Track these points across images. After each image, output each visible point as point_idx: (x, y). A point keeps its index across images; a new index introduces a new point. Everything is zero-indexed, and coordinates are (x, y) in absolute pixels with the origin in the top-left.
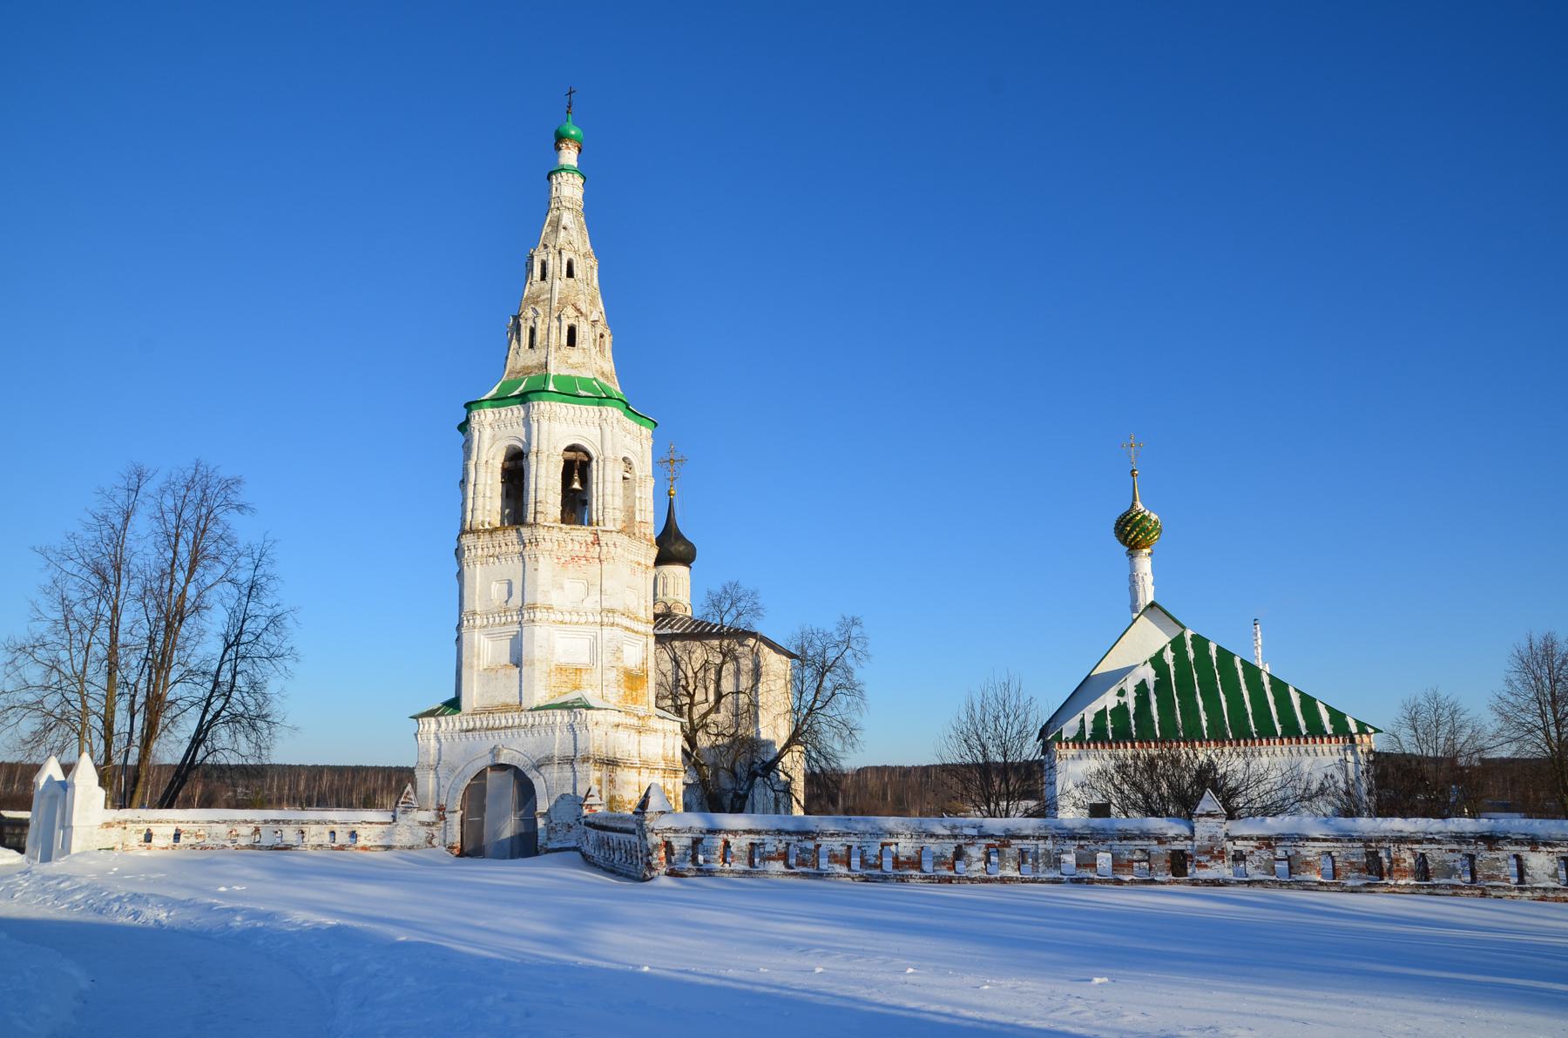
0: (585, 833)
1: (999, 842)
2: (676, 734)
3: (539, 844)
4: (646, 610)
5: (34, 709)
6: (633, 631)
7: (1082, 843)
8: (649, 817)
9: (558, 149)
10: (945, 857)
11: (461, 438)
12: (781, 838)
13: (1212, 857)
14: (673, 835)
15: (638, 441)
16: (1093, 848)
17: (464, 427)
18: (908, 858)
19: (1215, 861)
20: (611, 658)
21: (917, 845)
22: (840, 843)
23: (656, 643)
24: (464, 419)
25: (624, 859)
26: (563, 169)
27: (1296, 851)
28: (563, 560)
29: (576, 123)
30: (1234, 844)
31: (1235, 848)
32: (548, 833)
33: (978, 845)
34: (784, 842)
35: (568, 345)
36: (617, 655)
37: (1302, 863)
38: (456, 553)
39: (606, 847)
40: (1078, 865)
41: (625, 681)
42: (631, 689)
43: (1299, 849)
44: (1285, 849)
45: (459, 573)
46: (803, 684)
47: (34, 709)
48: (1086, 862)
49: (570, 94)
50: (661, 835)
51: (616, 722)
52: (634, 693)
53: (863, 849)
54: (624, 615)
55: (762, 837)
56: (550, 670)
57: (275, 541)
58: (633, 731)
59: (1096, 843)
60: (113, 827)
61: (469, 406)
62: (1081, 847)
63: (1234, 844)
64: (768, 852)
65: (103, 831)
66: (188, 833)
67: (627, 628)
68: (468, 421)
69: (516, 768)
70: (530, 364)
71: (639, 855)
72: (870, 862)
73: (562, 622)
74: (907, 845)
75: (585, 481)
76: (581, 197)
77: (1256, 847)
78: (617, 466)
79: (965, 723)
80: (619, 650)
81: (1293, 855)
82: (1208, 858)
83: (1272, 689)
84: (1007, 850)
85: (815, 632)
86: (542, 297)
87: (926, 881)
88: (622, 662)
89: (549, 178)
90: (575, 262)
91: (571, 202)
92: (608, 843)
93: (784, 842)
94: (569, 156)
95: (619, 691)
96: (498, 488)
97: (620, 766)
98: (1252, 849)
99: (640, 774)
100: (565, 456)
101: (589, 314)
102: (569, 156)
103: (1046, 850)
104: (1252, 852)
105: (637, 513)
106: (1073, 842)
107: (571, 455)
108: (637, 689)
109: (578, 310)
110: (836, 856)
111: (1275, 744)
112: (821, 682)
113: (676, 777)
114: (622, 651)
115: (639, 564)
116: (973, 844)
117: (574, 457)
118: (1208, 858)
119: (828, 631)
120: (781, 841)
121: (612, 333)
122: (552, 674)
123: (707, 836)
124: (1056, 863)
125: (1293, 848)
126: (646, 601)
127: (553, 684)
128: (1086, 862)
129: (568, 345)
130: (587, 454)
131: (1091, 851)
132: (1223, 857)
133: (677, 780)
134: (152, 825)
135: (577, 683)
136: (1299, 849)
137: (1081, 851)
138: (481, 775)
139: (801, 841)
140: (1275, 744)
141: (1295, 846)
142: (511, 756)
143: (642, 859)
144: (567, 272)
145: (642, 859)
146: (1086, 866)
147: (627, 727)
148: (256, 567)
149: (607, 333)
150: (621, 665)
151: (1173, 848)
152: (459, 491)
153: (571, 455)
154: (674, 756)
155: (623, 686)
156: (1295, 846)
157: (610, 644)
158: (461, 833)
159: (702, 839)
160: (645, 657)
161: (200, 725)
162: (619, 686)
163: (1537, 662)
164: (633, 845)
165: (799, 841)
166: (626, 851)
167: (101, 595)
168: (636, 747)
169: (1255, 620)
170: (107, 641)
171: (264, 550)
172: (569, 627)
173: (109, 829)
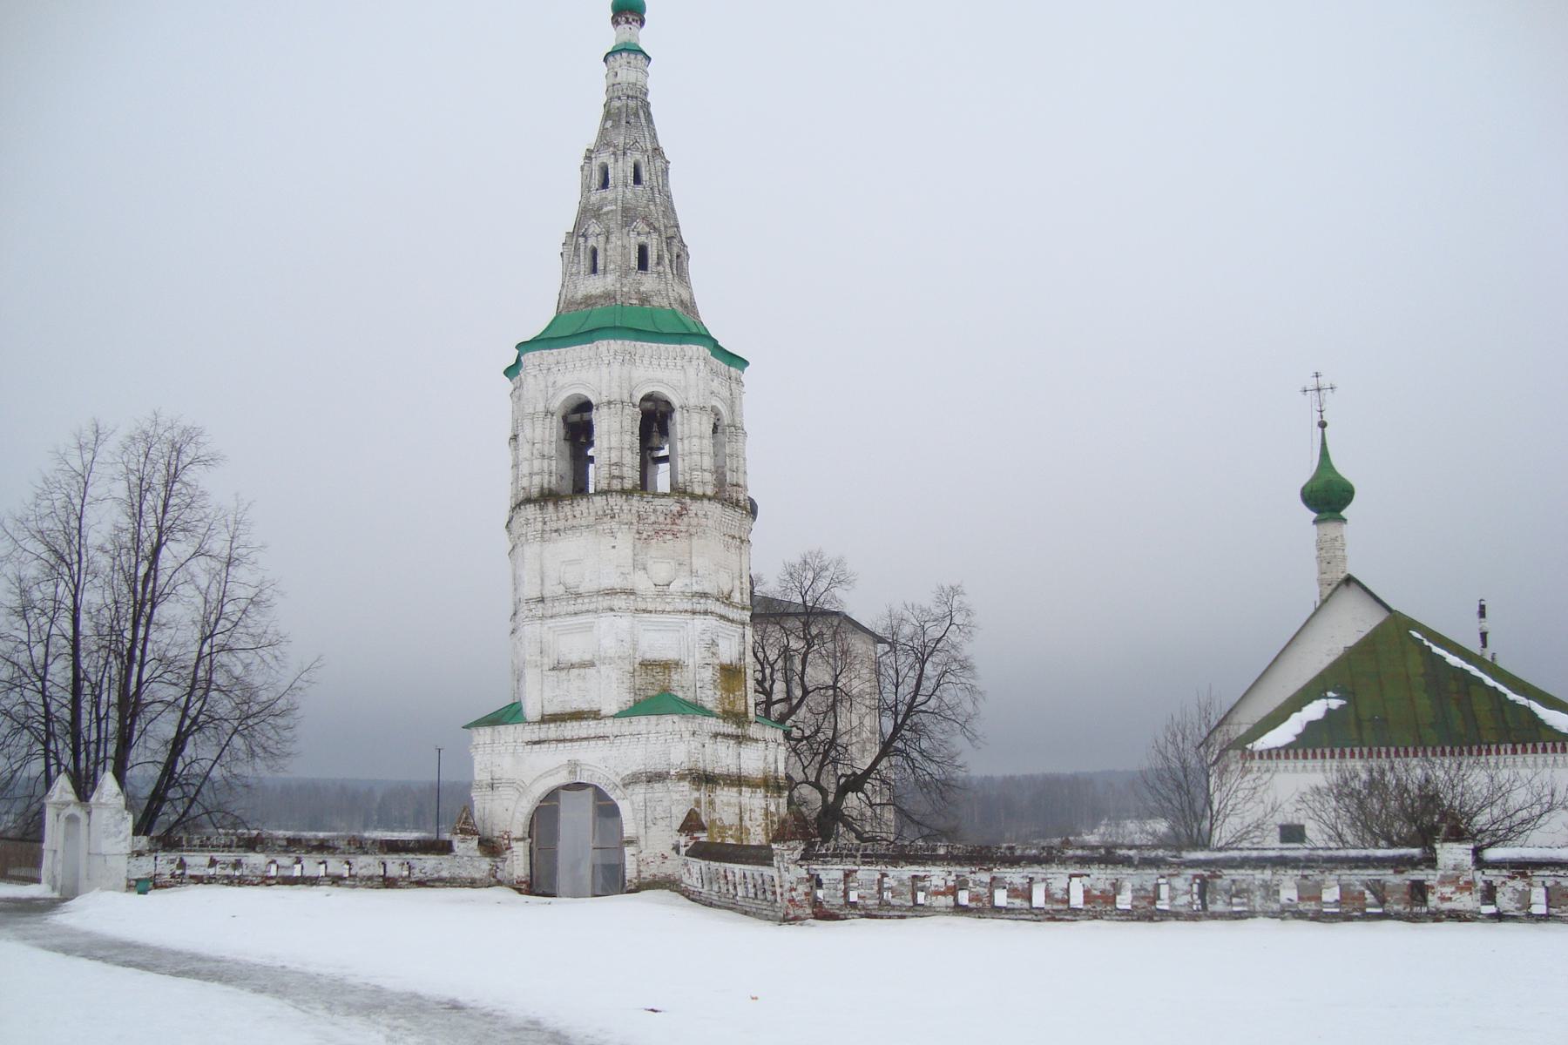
0: (686, 865)
1: (1208, 873)
2: (779, 744)
3: (627, 878)
4: (742, 594)
5: (1222, 824)
6: (728, 620)
7: (1307, 872)
10: (1145, 890)
11: (508, 386)
12: (950, 869)
13: (1457, 888)
14: (821, 867)
15: (727, 386)
16: (1319, 878)
18: (1103, 892)
19: (1461, 893)
20: (706, 654)
21: (1113, 877)
22: (1022, 875)
27: (1556, 881)
28: (644, 535)
30: (1483, 873)
31: (1484, 878)
32: (638, 865)
33: (1184, 876)
34: (953, 874)
36: (713, 650)
37: (1563, 895)
39: (722, 881)
40: (1300, 898)
41: (722, 681)
42: (728, 690)
43: (1559, 880)
44: (1543, 879)
46: (898, 675)
47: (1222, 824)
48: (1310, 893)
50: (806, 867)
52: (731, 696)
53: (1049, 881)
54: (719, 600)
55: (927, 868)
56: (634, 670)
57: (655, 585)
58: (733, 742)
59: (1322, 872)
60: (143, 855)
62: (1305, 877)
63: (1483, 873)
64: (936, 886)
65: (133, 860)
66: (224, 864)
67: (722, 617)
69: (596, 787)
70: (593, 293)
71: (778, 890)
72: (1056, 896)
73: (644, 611)
74: (1100, 876)
77: (1509, 877)
78: (705, 418)
79: (131, 574)
80: (714, 643)
81: (1552, 887)
82: (1453, 889)
83: (1467, 672)
84: (1218, 881)
85: (910, 607)
86: (605, 209)
87: (1122, 918)
88: (718, 658)
92: (726, 877)
93: (953, 874)
95: (715, 694)
97: (719, 784)
98: (1504, 879)
99: (740, 794)
100: (643, 407)
101: (662, 229)
103: (1263, 880)
104: (1504, 883)
105: (728, 474)
106: (1296, 872)
108: (734, 691)
110: (1015, 890)
111: (1506, 753)
112: (922, 670)
113: (780, 797)
114: (718, 646)
115: (734, 537)
116: (1177, 875)
117: (653, 408)
118: (1453, 889)
119: (925, 606)
120: (950, 873)
122: (636, 674)
123: (862, 867)
124: (1271, 891)
125: (1552, 878)
126: (741, 583)
127: (637, 687)
128: (1310, 893)
131: (1316, 881)
132: (1470, 889)
133: (781, 800)
134: (184, 854)
135: (666, 684)
136: (1559, 880)
137: (1305, 881)
138: (552, 795)
139: (974, 873)
140: (1506, 753)
141: (1555, 876)
142: (590, 773)
143: (782, 895)
145: (782, 895)
146: (1310, 899)
147: (726, 736)
148: (233, 538)
150: (717, 662)
151: (1413, 878)
154: (776, 769)
155: (719, 687)
156: (1555, 876)
157: (703, 637)
159: (856, 871)
160: (742, 650)
161: (179, 732)
162: (715, 687)
164: (768, 880)
165: (972, 873)
166: (755, 886)
168: (735, 761)
169: (1481, 600)
170: (70, 633)
171: (239, 516)
172: (654, 617)
173: (140, 858)
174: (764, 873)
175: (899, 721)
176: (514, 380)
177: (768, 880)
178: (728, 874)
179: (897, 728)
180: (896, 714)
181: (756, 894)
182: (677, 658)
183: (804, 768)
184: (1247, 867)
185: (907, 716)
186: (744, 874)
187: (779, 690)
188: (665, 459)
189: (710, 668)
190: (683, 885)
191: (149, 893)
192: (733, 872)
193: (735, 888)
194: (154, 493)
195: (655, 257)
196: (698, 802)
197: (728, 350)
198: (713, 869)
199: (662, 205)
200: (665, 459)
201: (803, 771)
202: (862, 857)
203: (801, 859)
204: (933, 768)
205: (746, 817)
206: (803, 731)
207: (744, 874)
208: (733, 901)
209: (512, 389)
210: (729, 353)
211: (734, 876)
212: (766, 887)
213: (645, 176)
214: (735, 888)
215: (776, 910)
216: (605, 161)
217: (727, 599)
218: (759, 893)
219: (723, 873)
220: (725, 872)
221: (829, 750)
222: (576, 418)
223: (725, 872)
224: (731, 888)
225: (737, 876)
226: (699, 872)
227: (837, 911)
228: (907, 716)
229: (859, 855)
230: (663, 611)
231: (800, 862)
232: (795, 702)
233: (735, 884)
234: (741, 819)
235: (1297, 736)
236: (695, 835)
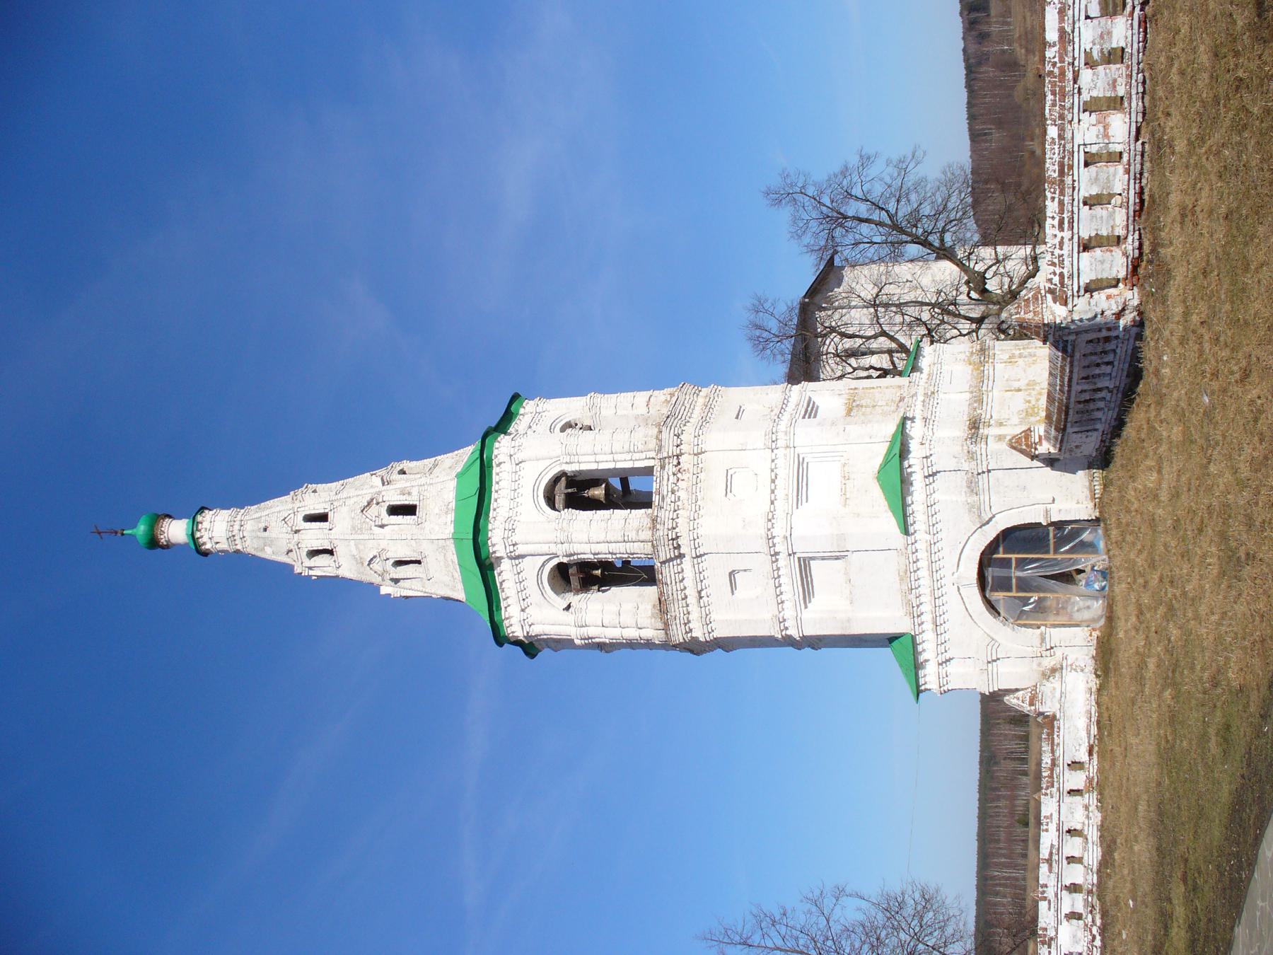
8: (1051, 317)
9: (168, 546)
11: (545, 654)
17: (530, 647)
23: (817, 379)
24: (519, 649)
25: (1108, 369)
26: (193, 535)
29: (134, 526)
35: (415, 515)
38: (697, 654)
39: (1092, 406)
45: (692, 652)
49: (99, 533)
51: (962, 431)
61: (499, 637)
64: (1097, 136)
68: (517, 643)
75: (593, 480)
76: (225, 511)
89: (206, 554)
90: (308, 513)
91: (232, 523)
92: (1087, 401)
94: (175, 531)
96: (553, 593)
102: (175, 531)
107: (559, 500)
109: (369, 504)
121: (399, 460)
129: (415, 515)
130: (556, 480)
144: (321, 521)
149: (399, 466)
152: (616, 653)
153: (559, 500)
158: (812, 286)
163: (1234, 748)
164: (1090, 348)
167: (1086, 810)
174: (1083, 352)
175: (909, 239)
176: (540, 647)
177: (1090, 348)
178: (1083, 400)
179: (916, 240)
180: (902, 243)
181: (1108, 363)
182: (1073, 838)
183: (961, 335)
184: (1034, 145)
185: (902, 231)
186: (1083, 378)
187: (882, 361)
188: (624, 482)
189: (848, 428)
190: (1094, 454)
191: (962, 42)
192: (1082, 391)
193: (1100, 390)
194: (1227, 66)
195: (404, 497)
196: (1000, 438)
197: (501, 415)
198: (1077, 417)
199: (1182, 417)
200: (624, 482)
201: (964, 335)
202: (1063, 230)
203: (1066, 304)
204: (954, 202)
205: (1016, 385)
206: (923, 336)
207: (1083, 378)
208: (1115, 391)
209: (549, 649)
210: (504, 415)
211: (1085, 391)
212: (1099, 349)
213: (319, 510)
214: (1100, 390)
215: (1127, 337)
216: (305, 553)
217: (772, 411)
218: (1106, 360)
219: (1082, 406)
220: (1079, 402)
221: (946, 308)
222: (575, 581)
223: (1079, 402)
224: (1100, 395)
225: (1086, 387)
226: (1080, 435)
227: (1130, 259)
228: (902, 231)
229: (1060, 235)
230: (375, 572)
231: (1070, 306)
232: (894, 345)
233: (1094, 390)
234: (1019, 390)
235: (968, 119)
236: (1037, 440)
